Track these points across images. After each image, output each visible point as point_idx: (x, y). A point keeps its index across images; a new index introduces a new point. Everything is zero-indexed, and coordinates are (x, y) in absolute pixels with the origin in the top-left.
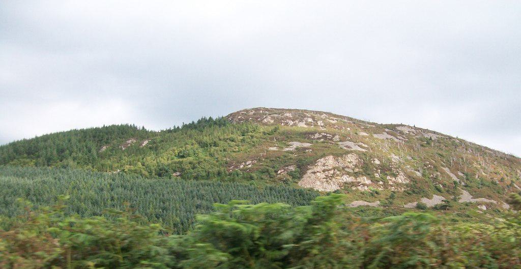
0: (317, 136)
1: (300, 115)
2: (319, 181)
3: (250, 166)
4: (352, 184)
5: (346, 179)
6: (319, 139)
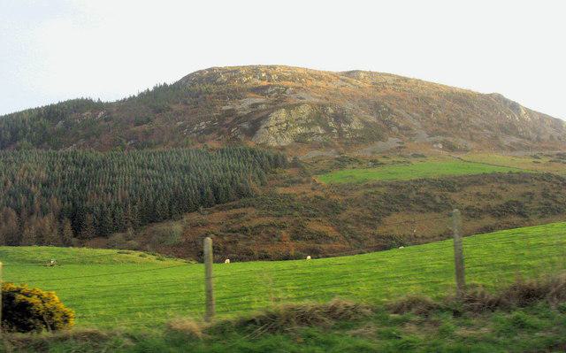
0: (270, 90)
1: (255, 70)
2: (273, 137)
3: (203, 127)
4: (305, 135)
5: (299, 130)
6: (271, 93)
